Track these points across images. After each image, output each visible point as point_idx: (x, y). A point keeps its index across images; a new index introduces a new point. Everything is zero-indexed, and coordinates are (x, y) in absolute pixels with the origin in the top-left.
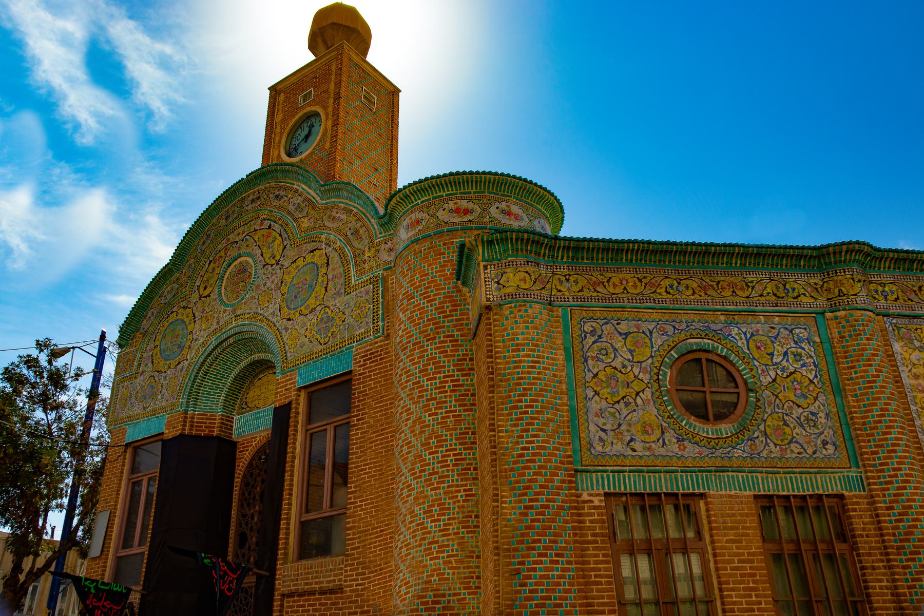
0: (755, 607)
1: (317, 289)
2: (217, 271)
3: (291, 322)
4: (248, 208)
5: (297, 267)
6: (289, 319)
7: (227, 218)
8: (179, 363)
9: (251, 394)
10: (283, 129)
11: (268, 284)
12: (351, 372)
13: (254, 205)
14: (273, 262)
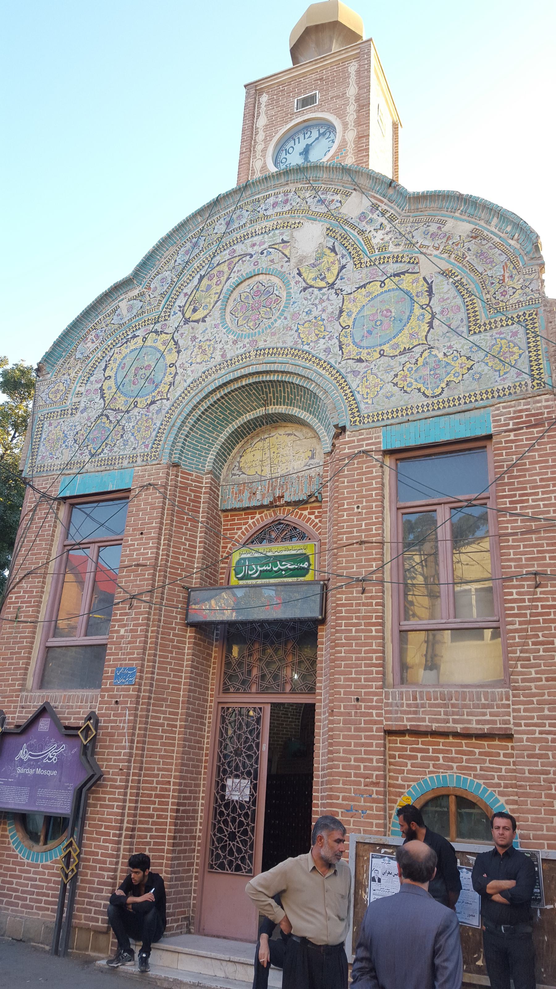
0: (352, 772)
1: (413, 322)
2: (216, 289)
3: (364, 364)
4: (268, 213)
5: (370, 293)
6: (360, 360)
7: (228, 224)
8: (153, 402)
9: (248, 457)
10: (266, 141)
11: (315, 313)
12: (129, 490)
13: (278, 209)
14: (322, 284)
